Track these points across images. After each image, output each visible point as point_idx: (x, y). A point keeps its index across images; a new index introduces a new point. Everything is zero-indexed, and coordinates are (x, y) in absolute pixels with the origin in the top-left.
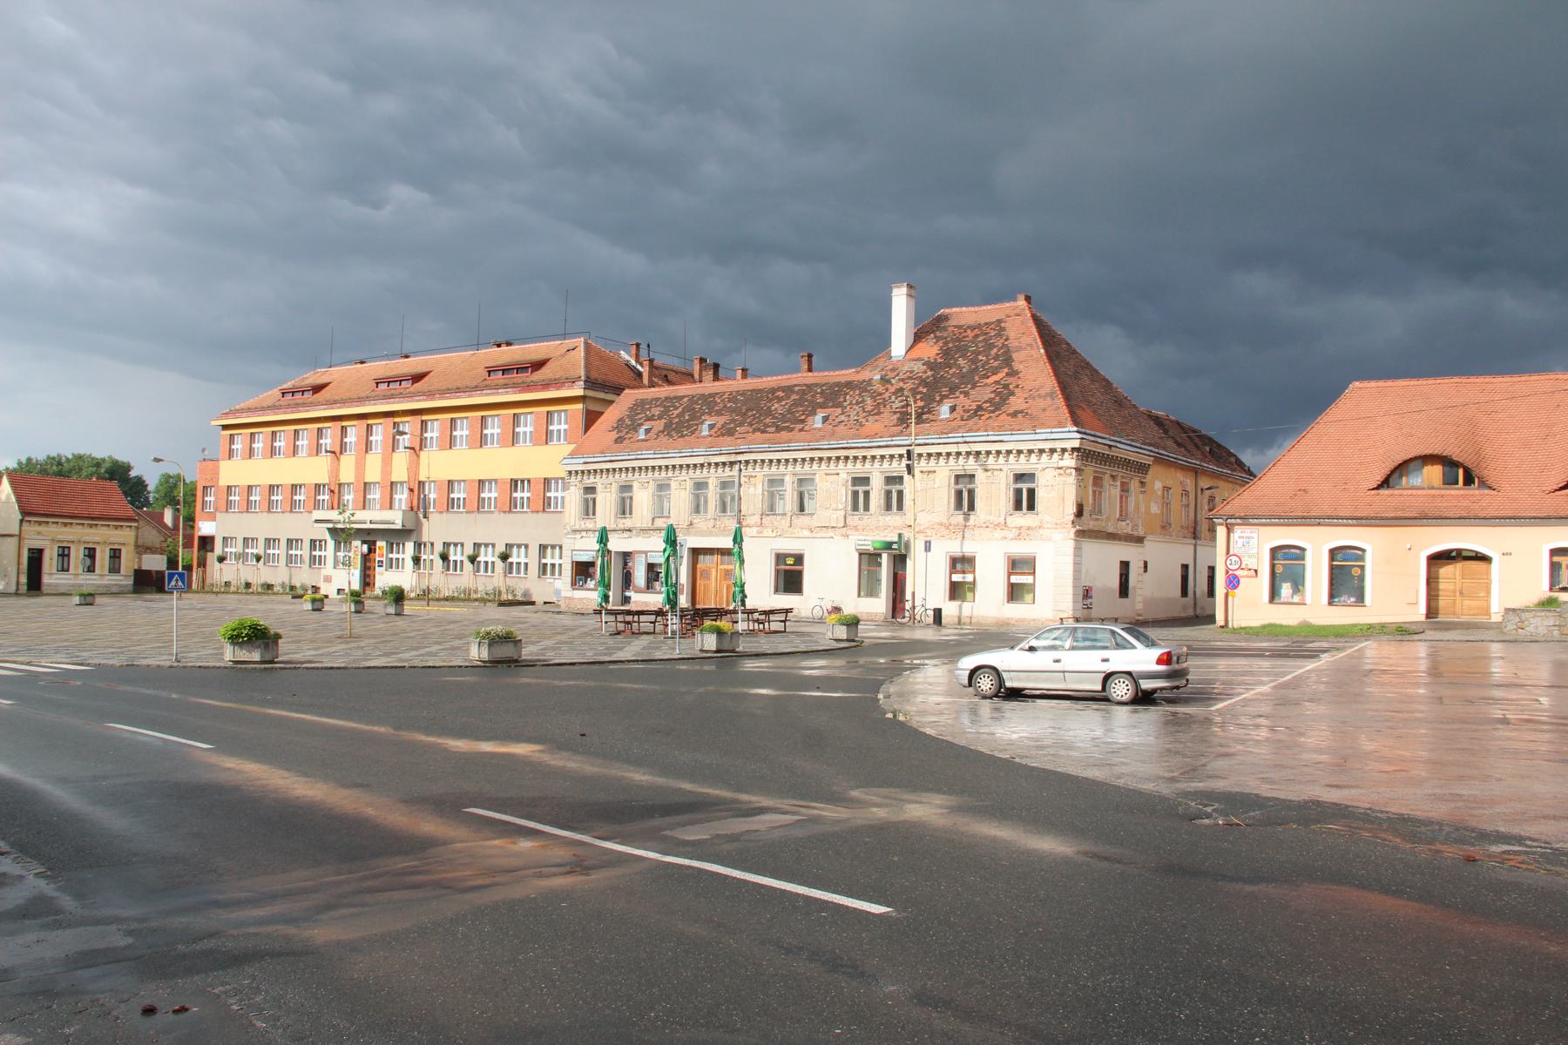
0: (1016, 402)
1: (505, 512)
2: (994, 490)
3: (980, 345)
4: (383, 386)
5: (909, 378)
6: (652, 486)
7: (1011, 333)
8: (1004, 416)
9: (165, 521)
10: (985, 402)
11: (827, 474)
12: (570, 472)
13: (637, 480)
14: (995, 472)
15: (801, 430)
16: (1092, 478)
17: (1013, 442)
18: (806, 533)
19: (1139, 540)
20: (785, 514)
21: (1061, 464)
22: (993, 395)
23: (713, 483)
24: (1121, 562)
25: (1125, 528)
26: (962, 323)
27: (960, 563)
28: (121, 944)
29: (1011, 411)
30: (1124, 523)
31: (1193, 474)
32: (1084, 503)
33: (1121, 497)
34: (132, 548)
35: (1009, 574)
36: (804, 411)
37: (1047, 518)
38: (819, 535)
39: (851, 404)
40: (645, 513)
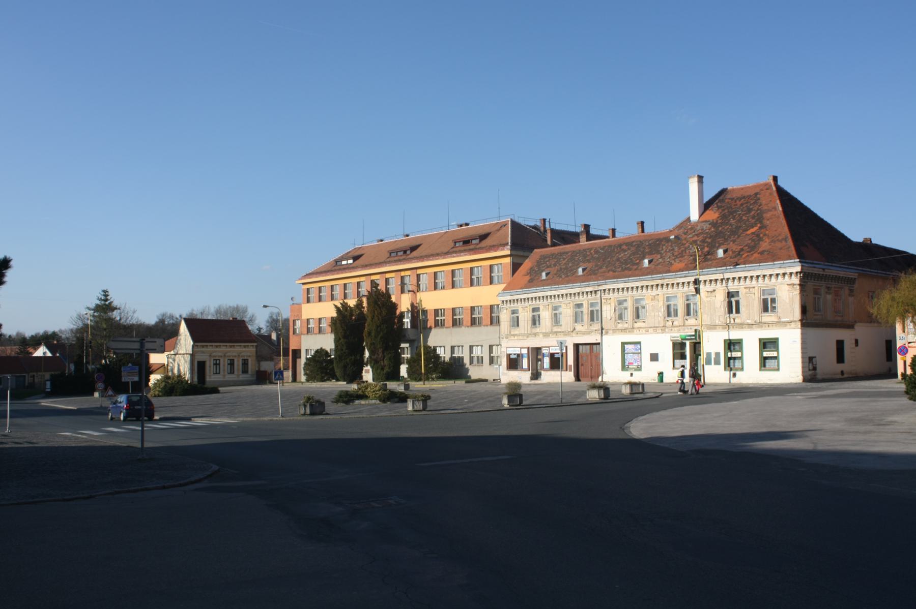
1: (468, 326)
4: (393, 255)
22: (750, 242)
26: (734, 196)
29: (760, 250)
34: (254, 358)
40: (547, 324)
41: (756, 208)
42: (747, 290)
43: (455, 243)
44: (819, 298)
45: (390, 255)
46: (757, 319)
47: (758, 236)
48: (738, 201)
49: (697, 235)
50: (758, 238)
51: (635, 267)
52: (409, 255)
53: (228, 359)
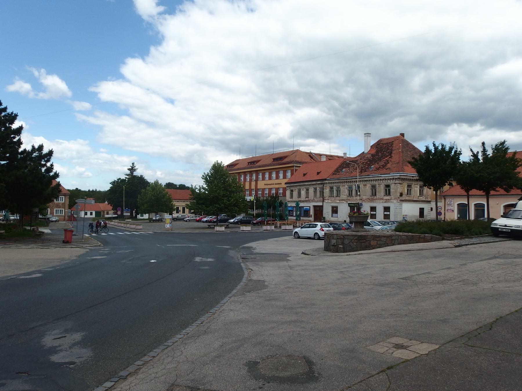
0: (389, 165)
3: (386, 149)
5: (367, 159)
6: (305, 189)
7: (394, 145)
9: (474, 190)
11: (342, 186)
12: (287, 186)
13: (302, 188)
14: (380, 185)
15: (338, 174)
17: (383, 176)
18: (338, 201)
20: (334, 197)
21: (396, 182)
22: (384, 164)
23: (59, 201)
24: (420, 208)
25: (421, 198)
30: (421, 197)
33: (420, 190)
35: (384, 212)
36: (340, 169)
37: (392, 197)
38: (342, 202)
39: (352, 167)
41: (390, 149)
44: (410, 190)
45: (249, 164)
46: (382, 197)
48: (384, 145)
49: (365, 160)
50: (387, 162)
51: (338, 173)
52: (255, 164)
53: (332, 216)
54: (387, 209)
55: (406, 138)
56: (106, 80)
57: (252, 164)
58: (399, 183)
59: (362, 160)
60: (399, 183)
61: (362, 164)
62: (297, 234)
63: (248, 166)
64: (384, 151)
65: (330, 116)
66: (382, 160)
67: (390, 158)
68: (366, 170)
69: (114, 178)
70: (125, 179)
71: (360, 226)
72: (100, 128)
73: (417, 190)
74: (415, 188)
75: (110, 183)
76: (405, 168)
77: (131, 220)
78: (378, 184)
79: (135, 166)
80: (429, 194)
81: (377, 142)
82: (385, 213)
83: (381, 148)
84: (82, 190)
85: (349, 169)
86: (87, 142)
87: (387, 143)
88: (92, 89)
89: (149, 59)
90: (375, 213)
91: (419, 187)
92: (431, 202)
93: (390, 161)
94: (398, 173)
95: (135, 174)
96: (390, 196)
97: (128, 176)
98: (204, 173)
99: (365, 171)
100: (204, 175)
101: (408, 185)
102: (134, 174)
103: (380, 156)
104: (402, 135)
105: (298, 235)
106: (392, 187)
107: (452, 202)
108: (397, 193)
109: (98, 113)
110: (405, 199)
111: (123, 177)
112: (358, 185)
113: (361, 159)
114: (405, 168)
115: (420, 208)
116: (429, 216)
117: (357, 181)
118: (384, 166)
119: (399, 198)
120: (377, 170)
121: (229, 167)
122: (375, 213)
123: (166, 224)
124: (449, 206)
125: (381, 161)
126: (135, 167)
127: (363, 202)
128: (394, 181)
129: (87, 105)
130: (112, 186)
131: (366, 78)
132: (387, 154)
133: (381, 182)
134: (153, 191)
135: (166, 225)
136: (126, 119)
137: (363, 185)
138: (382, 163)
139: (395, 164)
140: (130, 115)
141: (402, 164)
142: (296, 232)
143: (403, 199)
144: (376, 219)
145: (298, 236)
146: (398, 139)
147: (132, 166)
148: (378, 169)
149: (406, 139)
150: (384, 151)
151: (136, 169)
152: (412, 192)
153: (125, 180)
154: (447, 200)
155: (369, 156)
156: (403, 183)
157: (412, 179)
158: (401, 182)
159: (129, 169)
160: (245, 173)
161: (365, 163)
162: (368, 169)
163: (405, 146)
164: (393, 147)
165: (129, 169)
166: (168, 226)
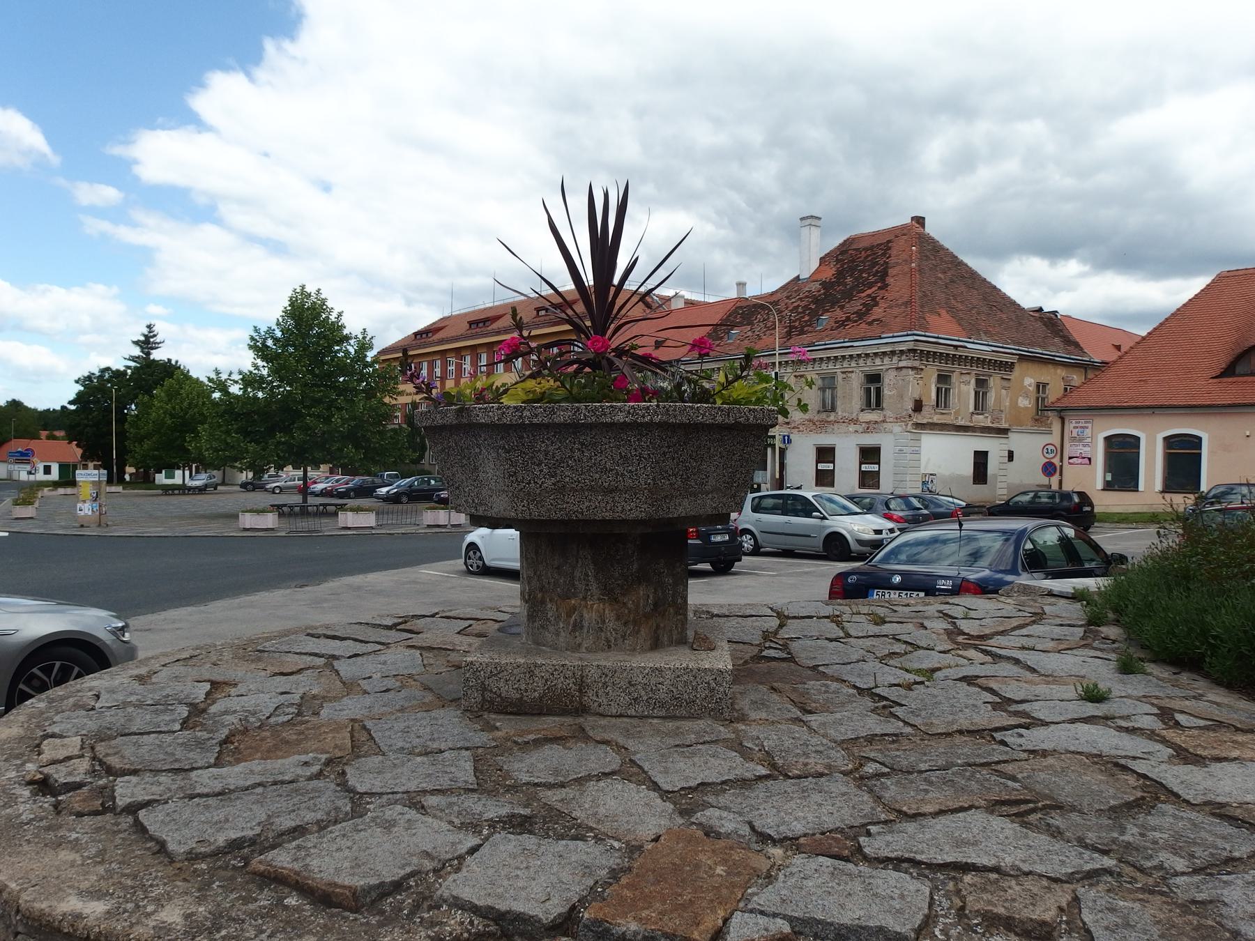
0: (877, 312)
2: (851, 391)
5: (807, 297)
7: (894, 252)
8: (863, 325)
10: (853, 314)
14: (849, 375)
16: (935, 376)
17: (859, 347)
19: (1004, 432)
21: (902, 364)
22: (861, 307)
24: (975, 452)
25: (981, 420)
27: (825, 454)
28: (1044, 837)
30: (981, 417)
31: (1083, 371)
32: (924, 399)
33: (977, 393)
35: (861, 464)
39: (759, 321)
41: (882, 262)
42: (845, 376)
43: (538, 312)
45: (470, 327)
47: (874, 299)
49: (800, 299)
50: (868, 308)
54: (870, 454)
55: (931, 229)
56: (153, 127)
57: (481, 325)
58: (913, 368)
59: (794, 300)
60: (913, 368)
61: (791, 311)
62: (478, 554)
63: (469, 332)
64: (862, 271)
65: (723, 233)
66: (855, 296)
67: (880, 288)
68: (806, 329)
69: (94, 363)
70: (125, 371)
71: (610, 595)
72: (145, 256)
73: (968, 393)
74: (962, 385)
75: (77, 382)
76: (931, 318)
77: (121, 487)
78: (843, 373)
79: (155, 333)
80: (1005, 406)
81: (840, 245)
82: (864, 468)
83: (853, 261)
84: (26, 404)
85: (751, 329)
86: (115, 290)
87: (872, 248)
88: (118, 151)
89: (261, 74)
90: (830, 466)
91: (973, 381)
92: (1010, 434)
93: (882, 299)
94: (909, 332)
95: (157, 355)
96: (882, 409)
97: (135, 361)
98: (255, 327)
99: (802, 332)
100: (255, 335)
101: (939, 375)
102: (152, 357)
103: (848, 287)
104: (918, 223)
105: (481, 558)
106: (889, 379)
107: (1088, 432)
108: (906, 399)
109: (139, 215)
110: (930, 421)
111: (118, 364)
112: (776, 373)
113: (788, 298)
114: (931, 318)
115: (975, 452)
116: (1003, 479)
117: (774, 364)
118: (861, 315)
119: (910, 416)
120: (838, 327)
121: (418, 337)
122: (830, 466)
123: (78, 502)
124: (1077, 446)
125: (851, 300)
126: (155, 336)
127: (792, 431)
128: (895, 359)
129: (109, 194)
130: (82, 388)
131: (816, 135)
132: (872, 279)
133: (853, 364)
134: (170, 400)
135: (79, 505)
136: (210, 232)
137: (795, 376)
138: (856, 305)
139: (897, 305)
140: (219, 222)
141: (922, 306)
142: (473, 546)
143: (925, 421)
144: (832, 485)
145: (480, 563)
146: (905, 231)
147: (146, 333)
148: (841, 324)
149: (932, 234)
150: (862, 271)
151: (159, 343)
152: (953, 399)
153: (124, 373)
154: (1070, 426)
155: (815, 287)
156: (923, 367)
157: (954, 355)
158: (917, 364)
159: (136, 343)
160: (457, 351)
161: (800, 310)
162: (809, 326)
163: (928, 254)
164: (890, 257)
165: (136, 343)
166: (86, 509)
